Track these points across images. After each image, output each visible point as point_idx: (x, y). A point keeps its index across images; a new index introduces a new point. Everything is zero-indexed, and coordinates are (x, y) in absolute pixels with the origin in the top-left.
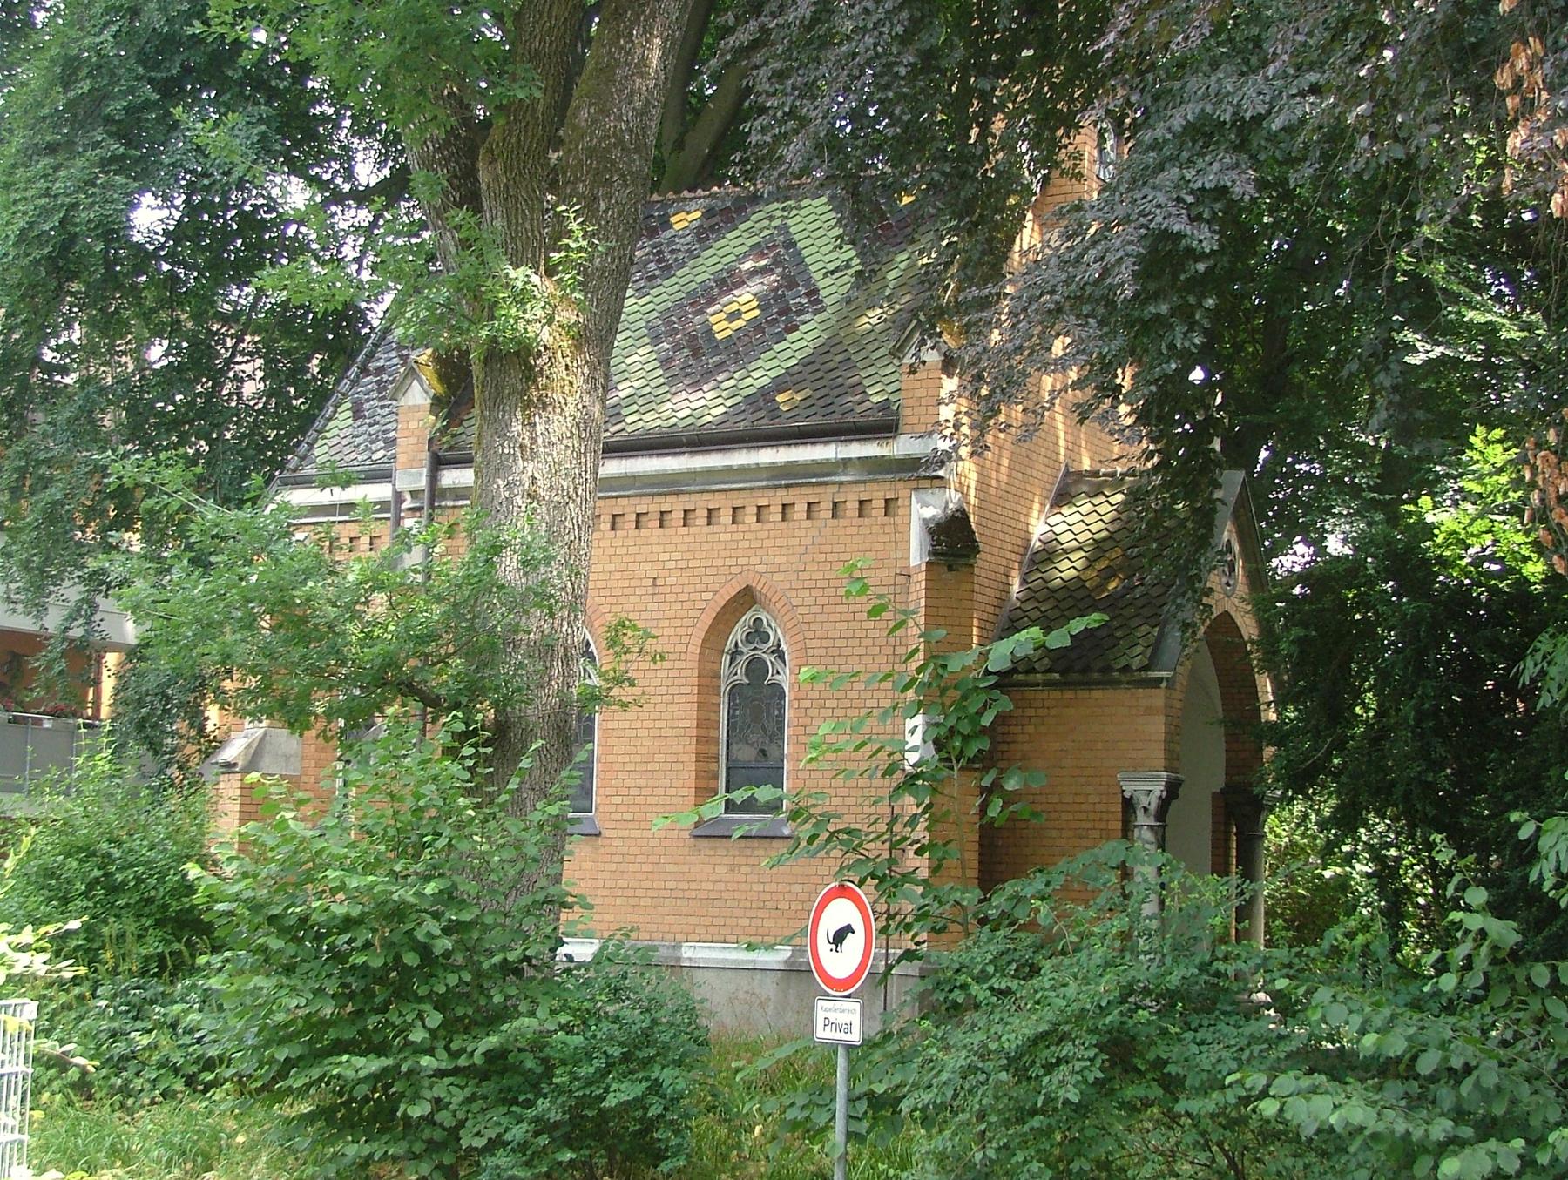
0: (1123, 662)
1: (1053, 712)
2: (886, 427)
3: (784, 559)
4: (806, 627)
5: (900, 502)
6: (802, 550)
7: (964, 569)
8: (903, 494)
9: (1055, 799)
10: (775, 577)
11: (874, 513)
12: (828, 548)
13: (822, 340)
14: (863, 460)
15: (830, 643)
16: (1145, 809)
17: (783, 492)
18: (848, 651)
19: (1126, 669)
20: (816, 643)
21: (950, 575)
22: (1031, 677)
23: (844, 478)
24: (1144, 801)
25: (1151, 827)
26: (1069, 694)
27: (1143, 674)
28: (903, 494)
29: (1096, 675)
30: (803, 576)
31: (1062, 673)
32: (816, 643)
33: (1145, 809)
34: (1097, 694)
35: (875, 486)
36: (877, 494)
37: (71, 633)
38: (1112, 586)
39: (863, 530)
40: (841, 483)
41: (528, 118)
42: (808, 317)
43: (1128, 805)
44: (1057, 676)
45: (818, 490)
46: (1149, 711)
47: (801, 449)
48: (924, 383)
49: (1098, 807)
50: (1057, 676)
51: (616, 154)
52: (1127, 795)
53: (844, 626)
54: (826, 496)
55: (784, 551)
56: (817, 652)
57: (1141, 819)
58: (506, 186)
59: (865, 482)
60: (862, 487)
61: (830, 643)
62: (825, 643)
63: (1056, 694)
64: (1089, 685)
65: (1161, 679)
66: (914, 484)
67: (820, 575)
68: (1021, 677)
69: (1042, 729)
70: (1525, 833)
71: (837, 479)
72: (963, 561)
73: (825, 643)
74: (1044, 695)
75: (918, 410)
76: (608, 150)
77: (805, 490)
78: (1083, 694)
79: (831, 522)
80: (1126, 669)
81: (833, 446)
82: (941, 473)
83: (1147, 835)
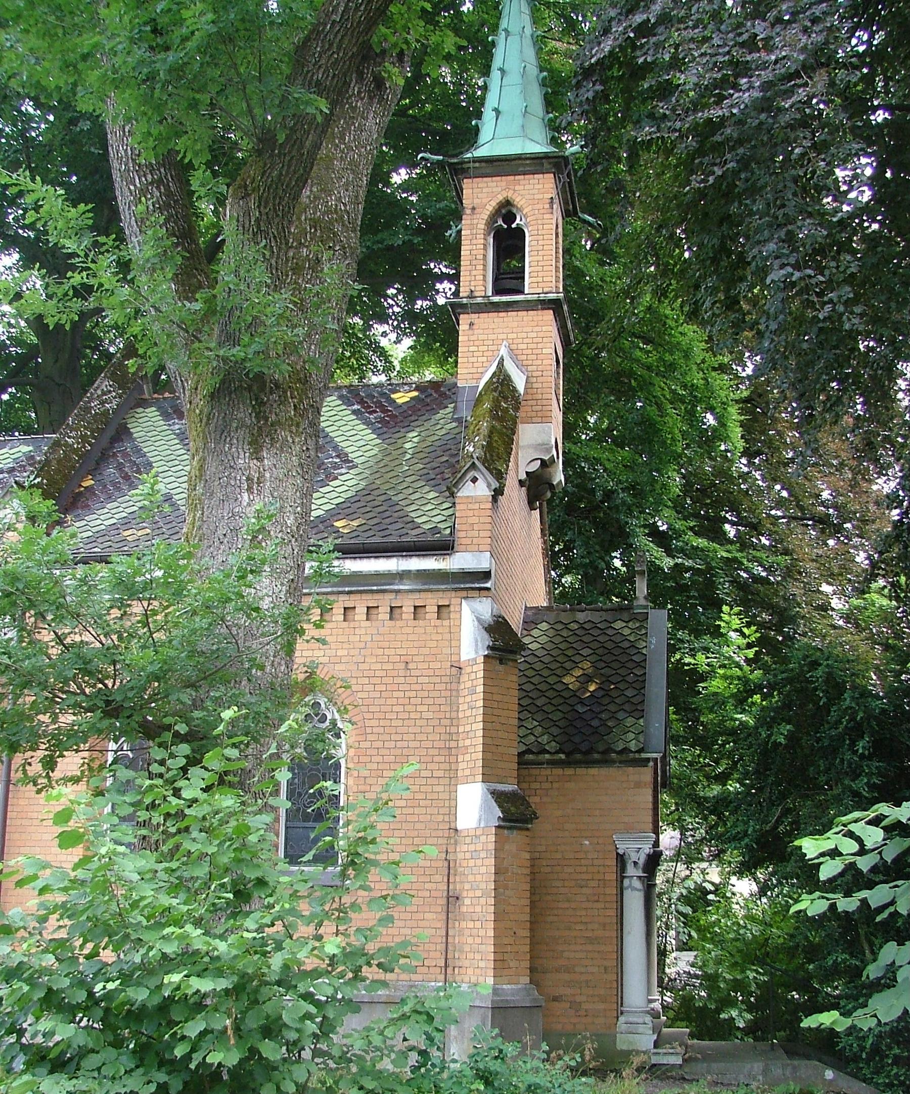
0: (620, 746)
1: (555, 785)
2: (445, 547)
3: (345, 652)
4: (364, 709)
5: (452, 608)
6: (362, 645)
7: (511, 663)
8: (454, 601)
9: (559, 856)
10: (337, 667)
11: (428, 616)
12: (386, 644)
13: (361, 487)
14: (419, 572)
15: (388, 723)
16: (635, 863)
17: (346, 597)
18: (405, 730)
19: (626, 750)
20: (374, 723)
21: (501, 668)
22: (541, 757)
23: (402, 587)
24: (634, 856)
25: (639, 877)
26: (569, 771)
27: (637, 756)
28: (454, 601)
29: (596, 756)
30: (361, 666)
31: (568, 755)
32: (374, 723)
33: (635, 863)
34: (593, 771)
35: (429, 595)
36: (431, 601)
37: (104, 384)
38: (592, 688)
39: (417, 630)
40: (398, 592)
41: (294, 153)
42: (343, 471)
43: (621, 860)
44: (563, 756)
45: (376, 596)
46: (638, 785)
47: (358, 562)
48: (476, 513)
49: (596, 862)
50: (563, 756)
51: (338, 228)
52: (621, 852)
53: (401, 708)
54: (384, 602)
55: (346, 646)
56: (375, 730)
57: (631, 871)
58: (258, 220)
59: (420, 591)
60: (417, 595)
61: (388, 723)
62: (382, 723)
63: (559, 771)
64: (589, 763)
65: (648, 760)
66: (464, 594)
67: (379, 666)
68: (531, 757)
69: (545, 799)
70: (269, 949)
71: (396, 587)
72: (511, 657)
73: (382, 723)
74: (548, 772)
75: (470, 534)
76: (331, 222)
77: (364, 596)
78: (580, 771)
79: (389, 623)
80: (626, 750)
81: (394, 560)
82: (488, 585)
83: (637, 884)
